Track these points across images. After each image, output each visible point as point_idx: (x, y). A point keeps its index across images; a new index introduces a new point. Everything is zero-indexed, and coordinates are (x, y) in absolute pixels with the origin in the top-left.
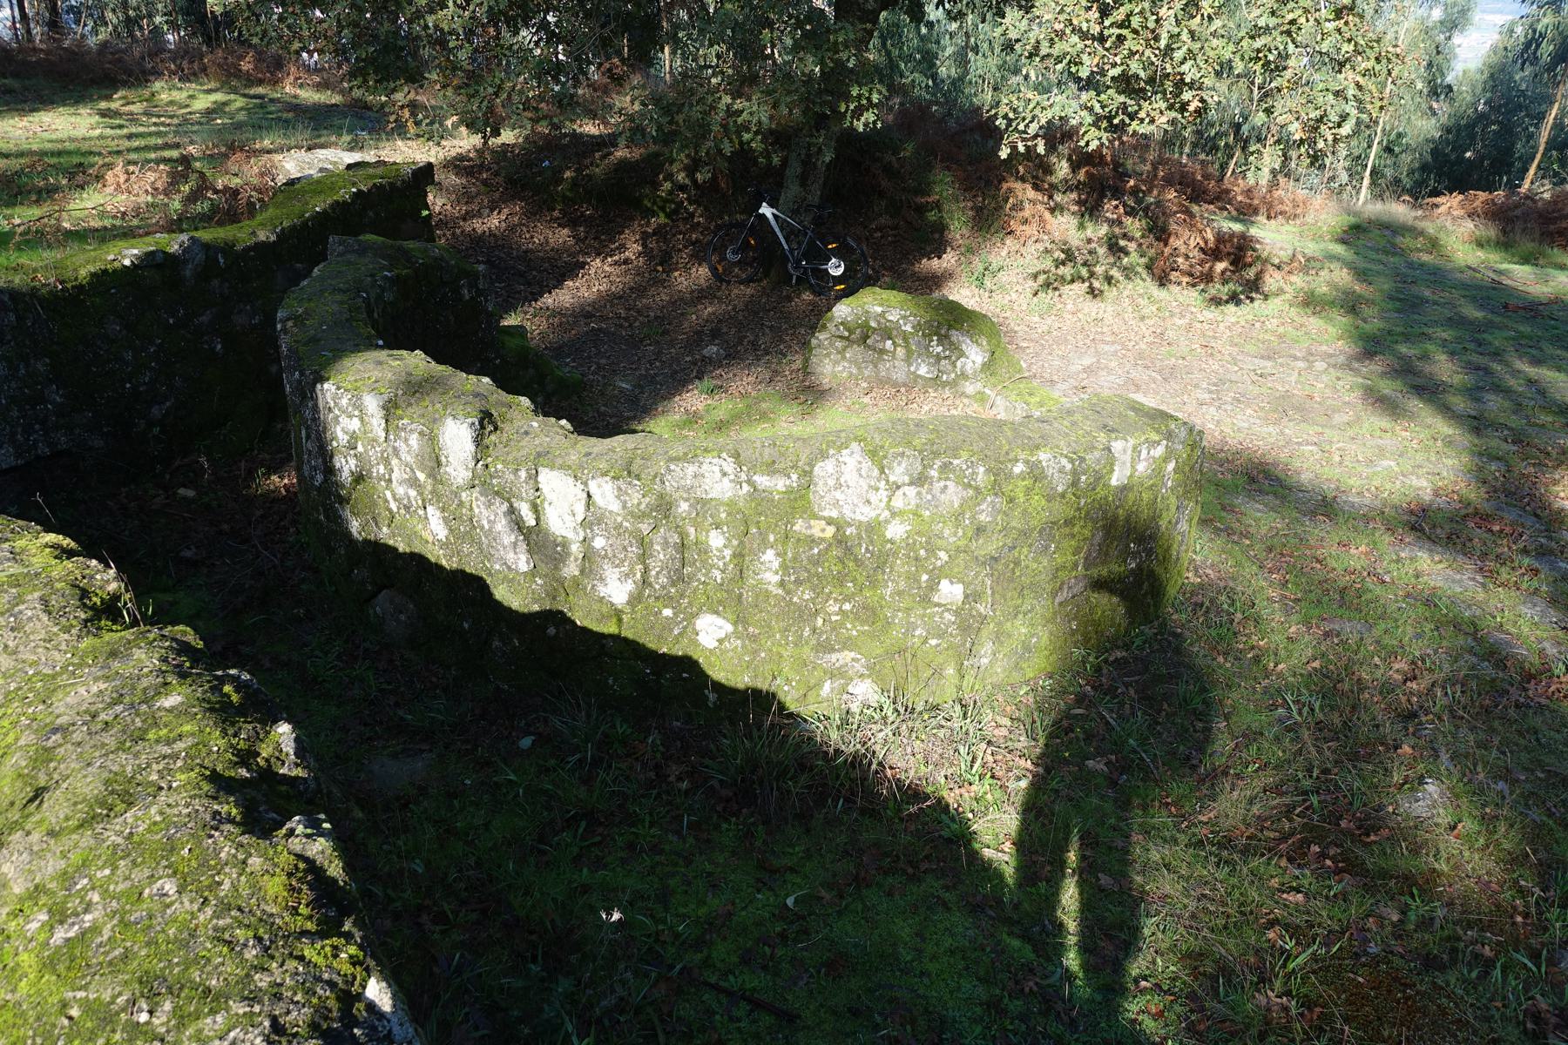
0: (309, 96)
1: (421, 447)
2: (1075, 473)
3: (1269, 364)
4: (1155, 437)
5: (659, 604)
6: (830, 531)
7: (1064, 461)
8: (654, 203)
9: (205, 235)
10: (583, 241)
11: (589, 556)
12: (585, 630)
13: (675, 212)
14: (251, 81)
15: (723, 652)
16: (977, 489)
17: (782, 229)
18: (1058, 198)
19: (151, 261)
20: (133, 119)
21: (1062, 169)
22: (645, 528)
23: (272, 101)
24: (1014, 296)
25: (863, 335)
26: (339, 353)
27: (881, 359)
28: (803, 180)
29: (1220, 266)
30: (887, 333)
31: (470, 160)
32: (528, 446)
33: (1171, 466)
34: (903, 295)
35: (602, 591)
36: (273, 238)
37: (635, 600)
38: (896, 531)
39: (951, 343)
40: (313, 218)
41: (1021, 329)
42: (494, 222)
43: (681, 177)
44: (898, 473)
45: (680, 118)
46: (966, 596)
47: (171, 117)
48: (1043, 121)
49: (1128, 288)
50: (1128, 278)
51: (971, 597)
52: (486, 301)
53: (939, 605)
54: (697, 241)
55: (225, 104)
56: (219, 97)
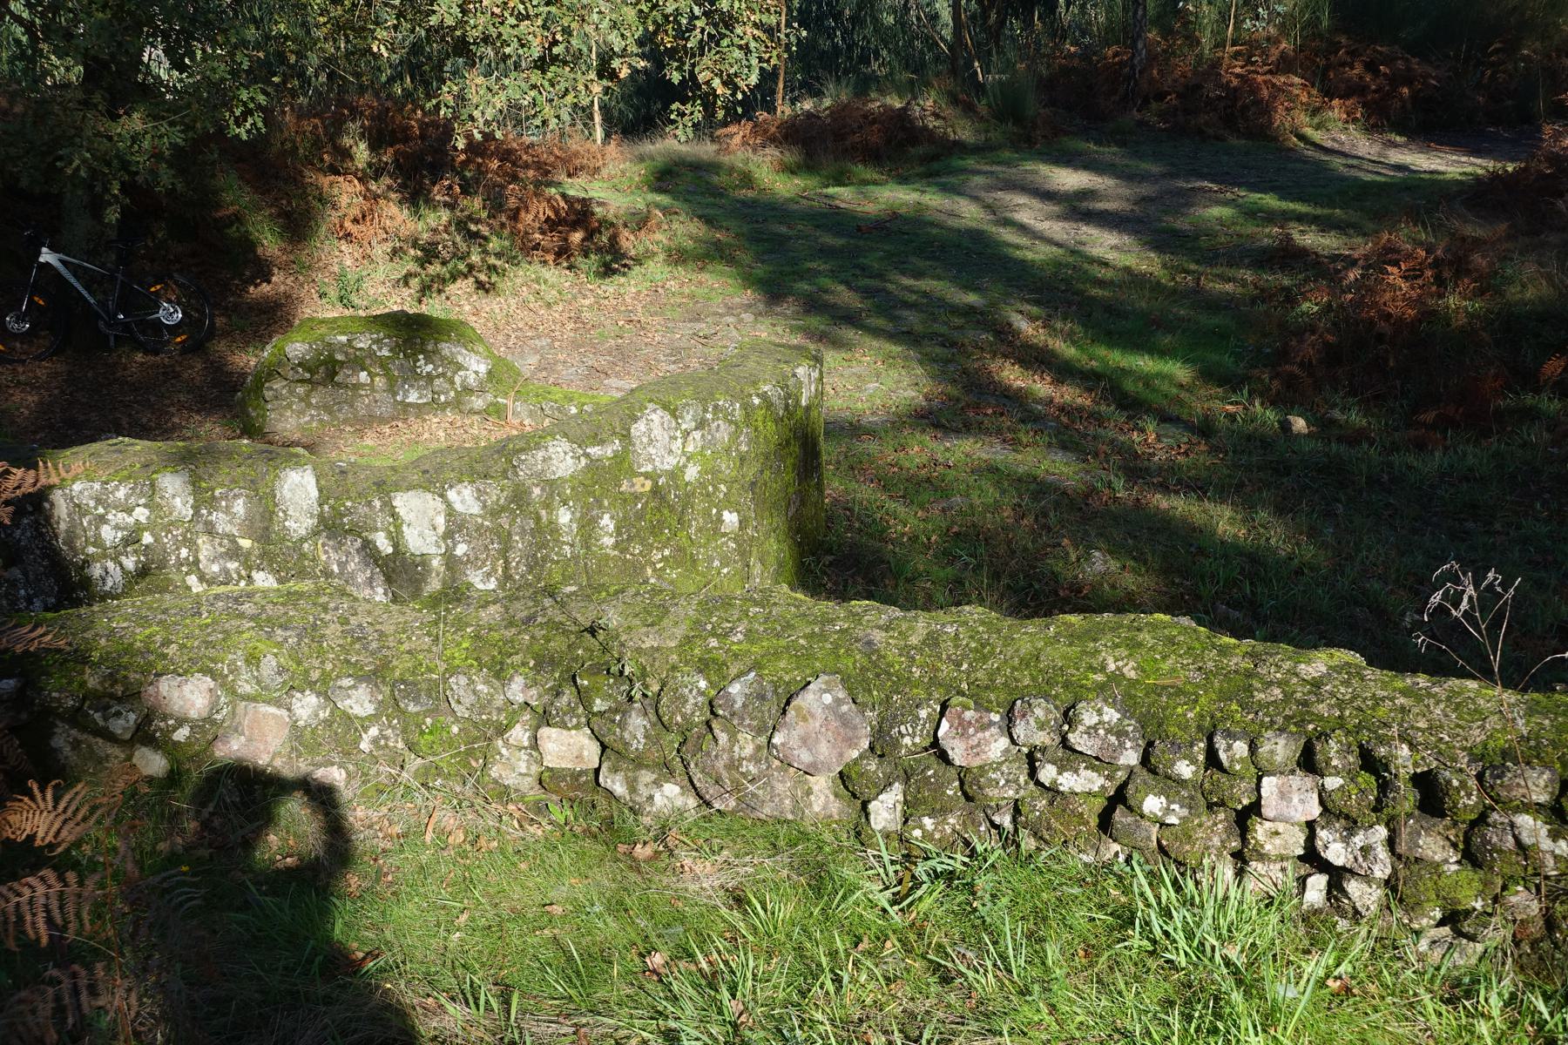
1: (248, 511)
6: (648, 484)
11: (450, 561)
27: (356, 396)
39: (443, 358)
44: (688, 423)
46: (740, 522)
51: (743, 523)
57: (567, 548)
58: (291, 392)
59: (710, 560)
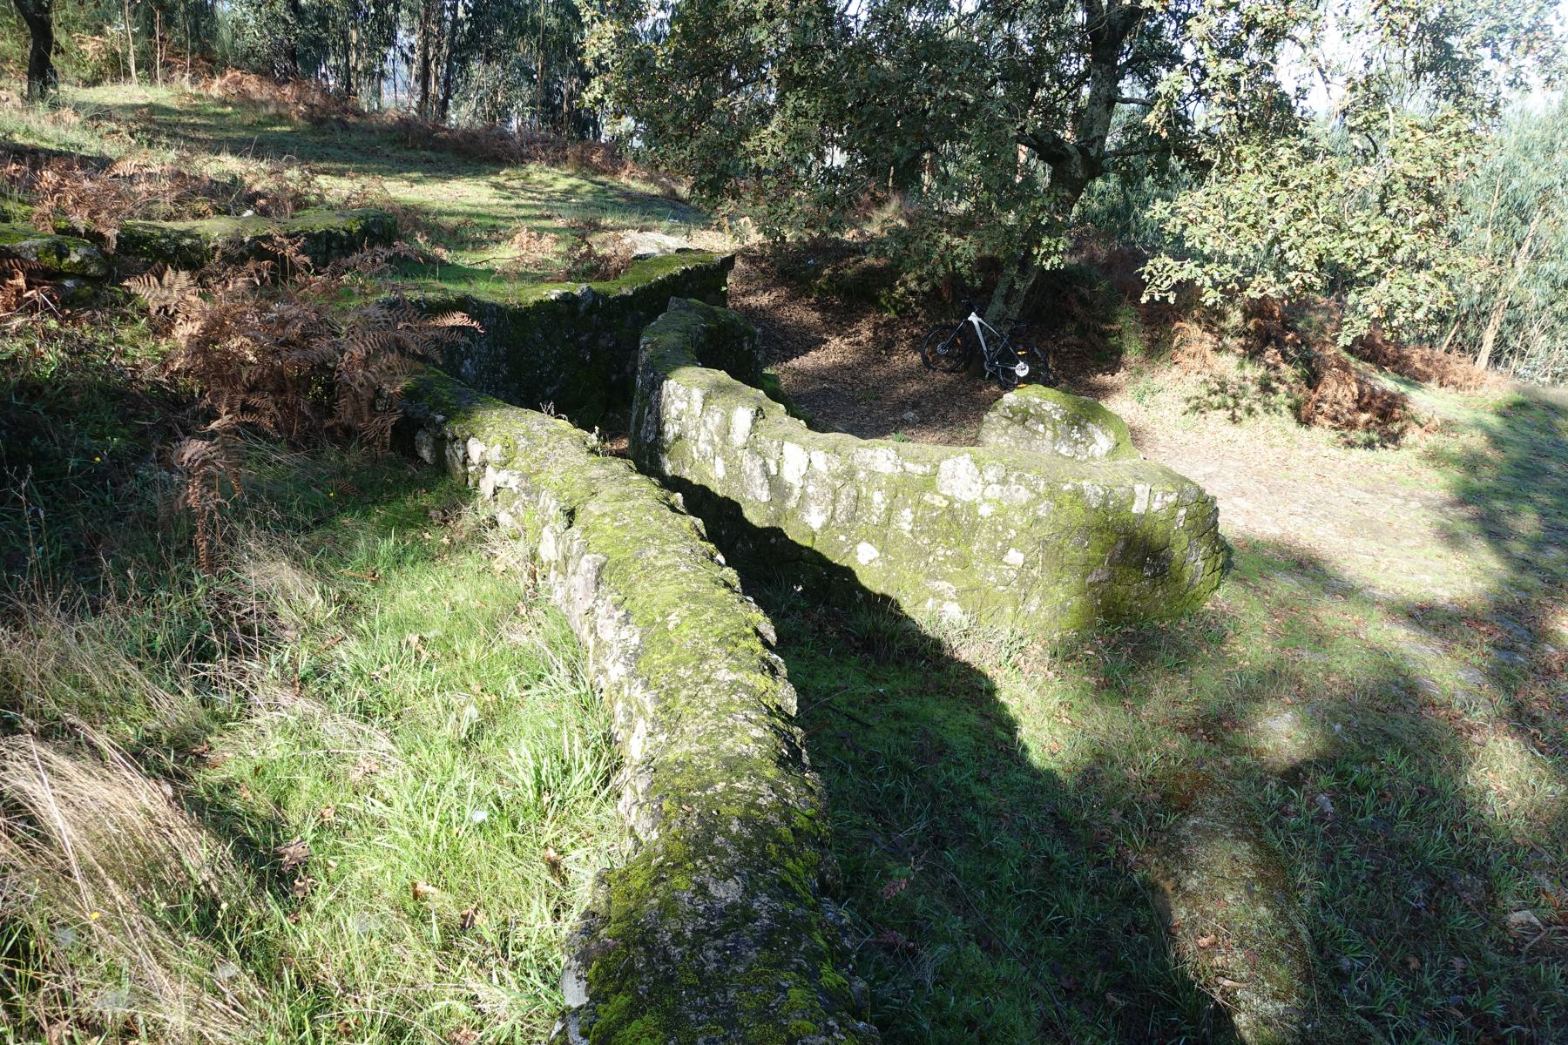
0: (637, 186)
2: (1106, 498)
3: (1369, 496)
4: (1170, 489)
6: (945, 503)
7: (1099, 489)
8: (889, 302)
9: (595, 286)
10: (829, 323)
11: (803, 497)
12: (793, 542)
13: (903, 311)
14: (598, 171)
15: (871, 568)
16: (1038, 494)
17: (984, 335)
18: (1227, 340)
19: (567, 299)
20: (515, 192)
21: (1235, 318)
22: (838, 484)
23: (611, 188)
24: (1166, 412)
25: (1022, 417)
26: (677, 365)
28: (1007, 300)
29: (1364, 417)
30: (1041, 418)
31: (754, 252)
32: (781, 430)
33: (1182, 512)
35: (807, 519)
36: (631, 293)
37: (825, 527)
38: (985, 511)
39: (1087, 433)
40: (656, 283)
41: (1163, 439)
42: (764, 300)
43: (913, 285)
44: (991, 475)
45: (912, 246)
47: (540, 193)
48: (1174, 281)
49: (1264, 419)
50: (1267, 411)
51: (1029, 564)
53: (1006, 564)
54: (917, 335)
55: (578, 187)
56: (574, 181)
58: (998, 422)
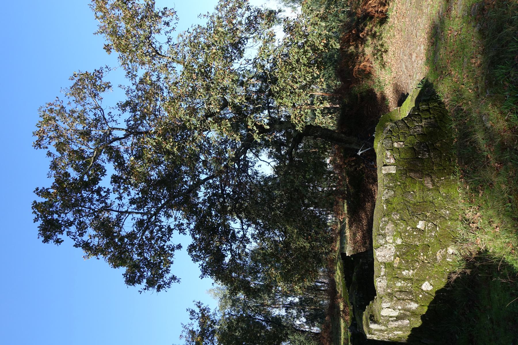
5: (418, 298)
6: (397, 258)
7: (385, 192)
16: (389, 220)
34: (375, 142)
37: (416, 302)
52: (369, 261)
53: (425, 228)
57: (408, 285)
59: (431, 236)
